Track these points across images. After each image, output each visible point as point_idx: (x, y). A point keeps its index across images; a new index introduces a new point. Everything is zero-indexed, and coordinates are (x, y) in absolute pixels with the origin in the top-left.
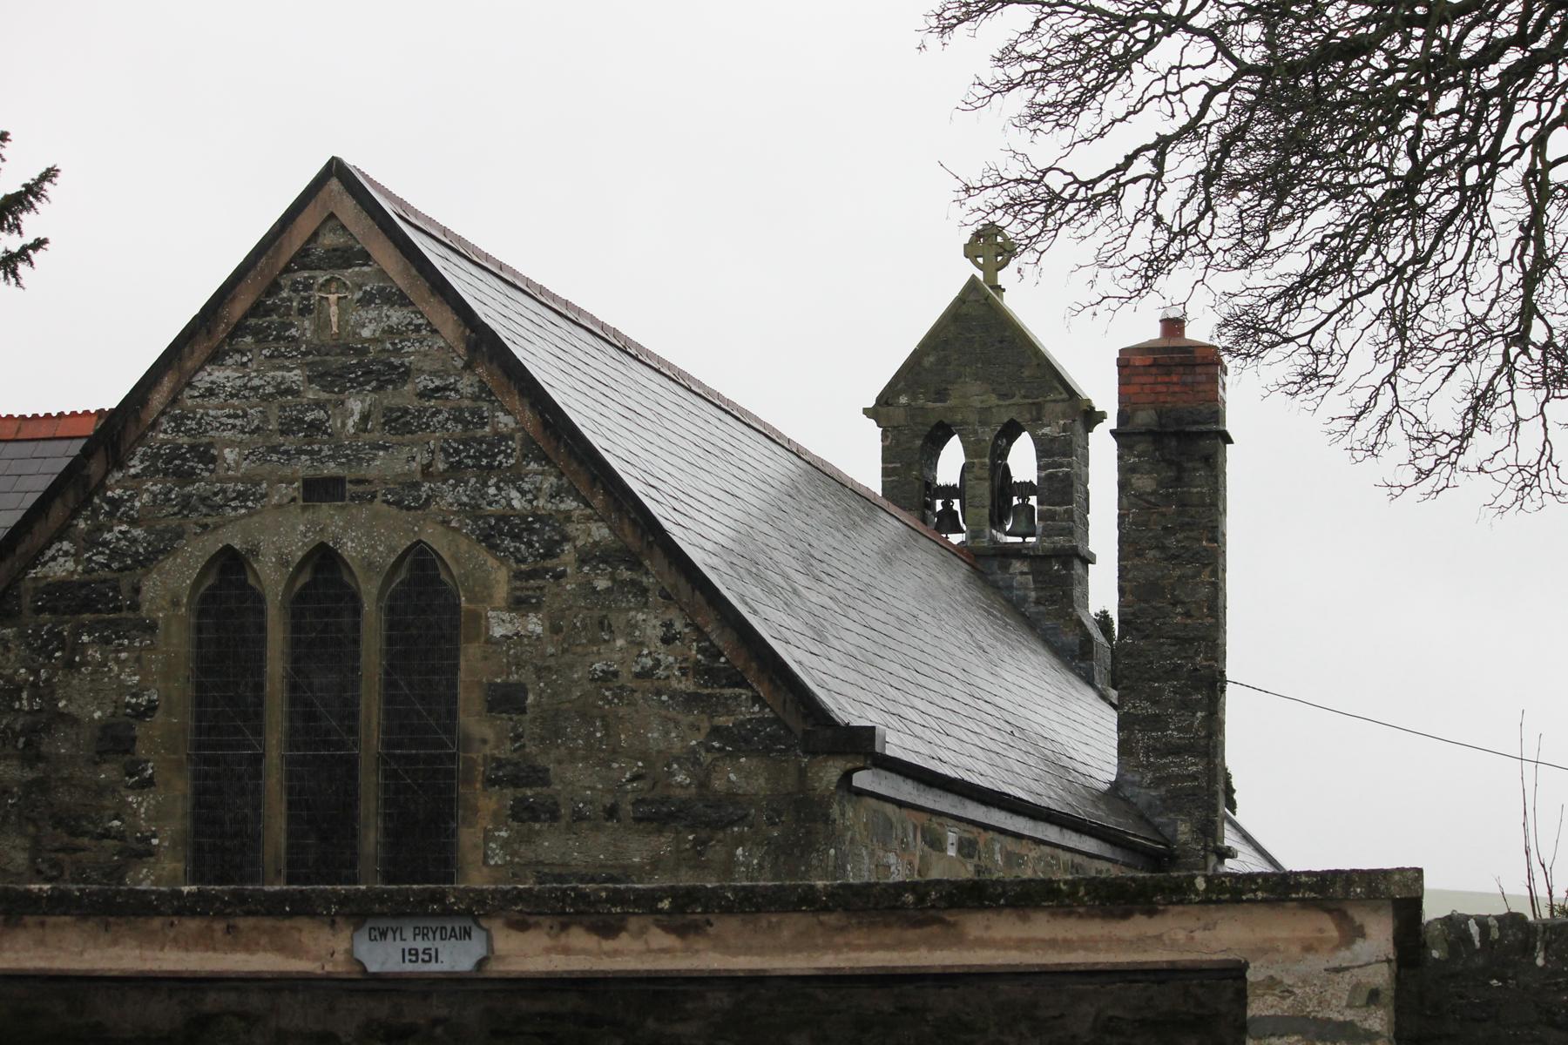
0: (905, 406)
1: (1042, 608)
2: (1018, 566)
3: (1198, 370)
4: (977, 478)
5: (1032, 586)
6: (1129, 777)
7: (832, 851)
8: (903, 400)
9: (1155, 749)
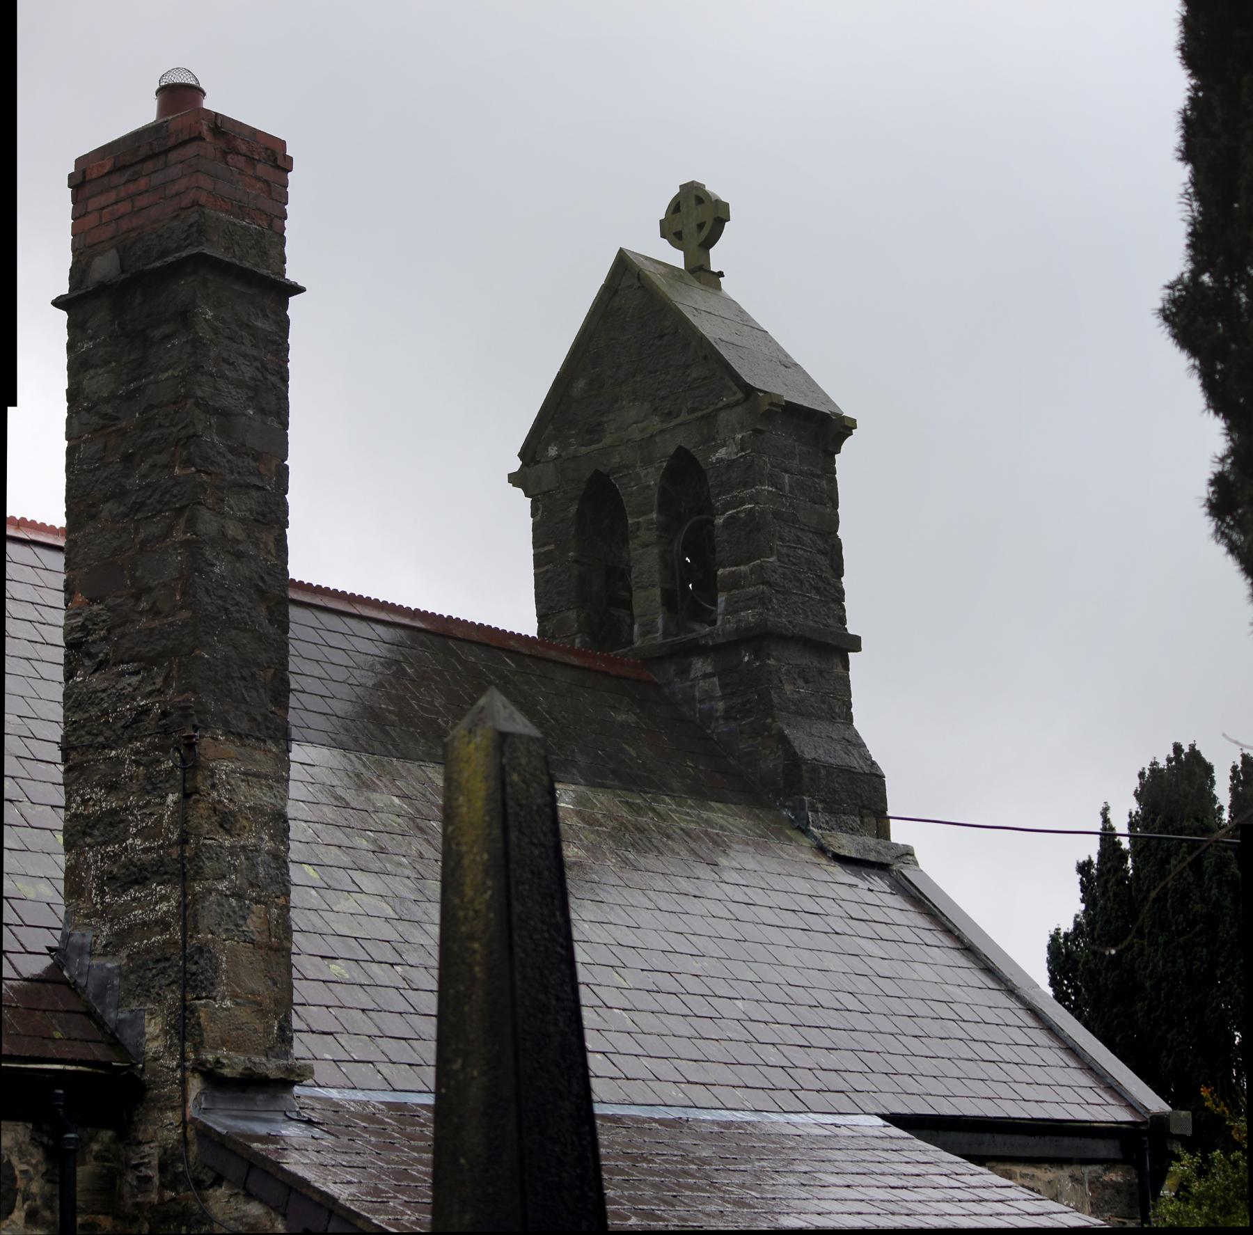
0: (555, 459)
1: (733, 724)
2: (700, 666)
3: (173, 156)
4: (644, 545)
5: (719, 693)
6: (76, 938)
7: (462, 1161)
8: (553, 451)
9: (112, 878)
